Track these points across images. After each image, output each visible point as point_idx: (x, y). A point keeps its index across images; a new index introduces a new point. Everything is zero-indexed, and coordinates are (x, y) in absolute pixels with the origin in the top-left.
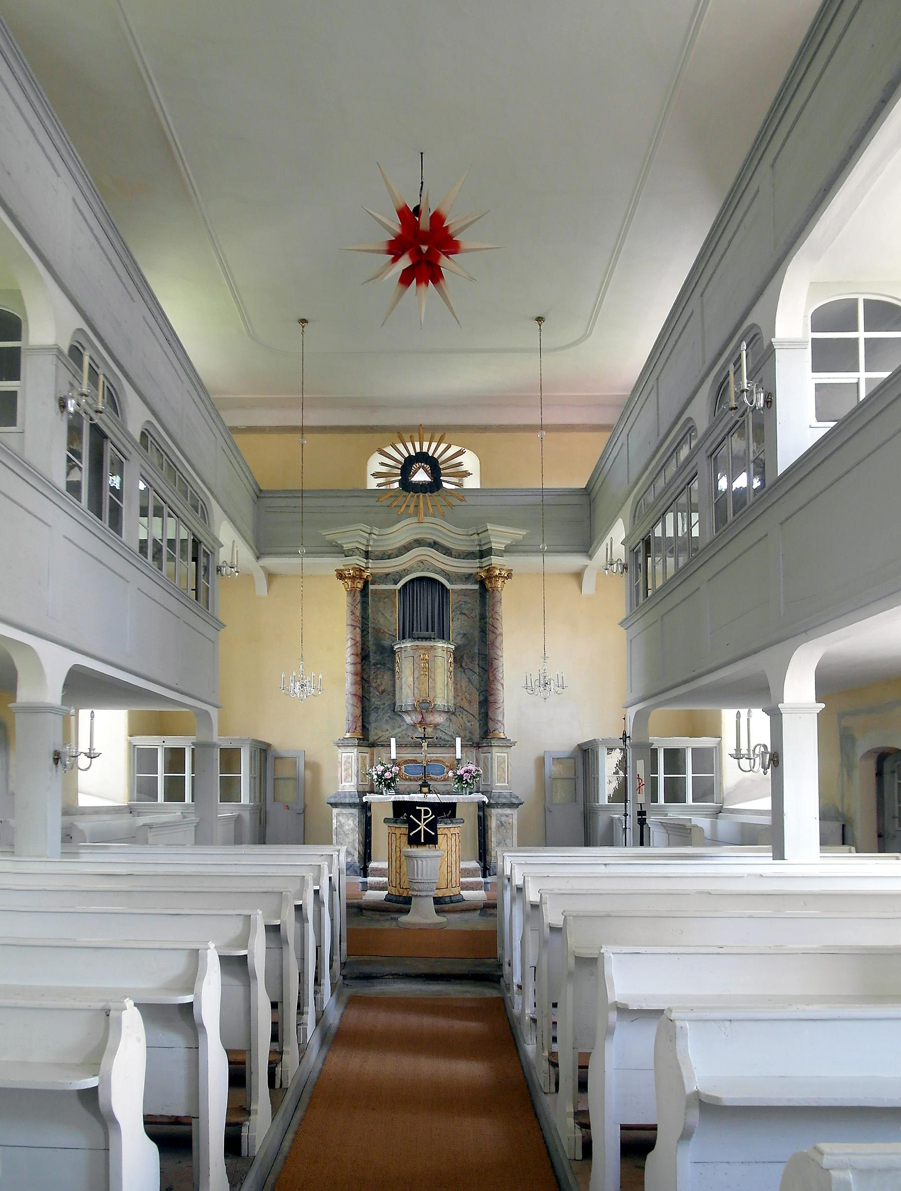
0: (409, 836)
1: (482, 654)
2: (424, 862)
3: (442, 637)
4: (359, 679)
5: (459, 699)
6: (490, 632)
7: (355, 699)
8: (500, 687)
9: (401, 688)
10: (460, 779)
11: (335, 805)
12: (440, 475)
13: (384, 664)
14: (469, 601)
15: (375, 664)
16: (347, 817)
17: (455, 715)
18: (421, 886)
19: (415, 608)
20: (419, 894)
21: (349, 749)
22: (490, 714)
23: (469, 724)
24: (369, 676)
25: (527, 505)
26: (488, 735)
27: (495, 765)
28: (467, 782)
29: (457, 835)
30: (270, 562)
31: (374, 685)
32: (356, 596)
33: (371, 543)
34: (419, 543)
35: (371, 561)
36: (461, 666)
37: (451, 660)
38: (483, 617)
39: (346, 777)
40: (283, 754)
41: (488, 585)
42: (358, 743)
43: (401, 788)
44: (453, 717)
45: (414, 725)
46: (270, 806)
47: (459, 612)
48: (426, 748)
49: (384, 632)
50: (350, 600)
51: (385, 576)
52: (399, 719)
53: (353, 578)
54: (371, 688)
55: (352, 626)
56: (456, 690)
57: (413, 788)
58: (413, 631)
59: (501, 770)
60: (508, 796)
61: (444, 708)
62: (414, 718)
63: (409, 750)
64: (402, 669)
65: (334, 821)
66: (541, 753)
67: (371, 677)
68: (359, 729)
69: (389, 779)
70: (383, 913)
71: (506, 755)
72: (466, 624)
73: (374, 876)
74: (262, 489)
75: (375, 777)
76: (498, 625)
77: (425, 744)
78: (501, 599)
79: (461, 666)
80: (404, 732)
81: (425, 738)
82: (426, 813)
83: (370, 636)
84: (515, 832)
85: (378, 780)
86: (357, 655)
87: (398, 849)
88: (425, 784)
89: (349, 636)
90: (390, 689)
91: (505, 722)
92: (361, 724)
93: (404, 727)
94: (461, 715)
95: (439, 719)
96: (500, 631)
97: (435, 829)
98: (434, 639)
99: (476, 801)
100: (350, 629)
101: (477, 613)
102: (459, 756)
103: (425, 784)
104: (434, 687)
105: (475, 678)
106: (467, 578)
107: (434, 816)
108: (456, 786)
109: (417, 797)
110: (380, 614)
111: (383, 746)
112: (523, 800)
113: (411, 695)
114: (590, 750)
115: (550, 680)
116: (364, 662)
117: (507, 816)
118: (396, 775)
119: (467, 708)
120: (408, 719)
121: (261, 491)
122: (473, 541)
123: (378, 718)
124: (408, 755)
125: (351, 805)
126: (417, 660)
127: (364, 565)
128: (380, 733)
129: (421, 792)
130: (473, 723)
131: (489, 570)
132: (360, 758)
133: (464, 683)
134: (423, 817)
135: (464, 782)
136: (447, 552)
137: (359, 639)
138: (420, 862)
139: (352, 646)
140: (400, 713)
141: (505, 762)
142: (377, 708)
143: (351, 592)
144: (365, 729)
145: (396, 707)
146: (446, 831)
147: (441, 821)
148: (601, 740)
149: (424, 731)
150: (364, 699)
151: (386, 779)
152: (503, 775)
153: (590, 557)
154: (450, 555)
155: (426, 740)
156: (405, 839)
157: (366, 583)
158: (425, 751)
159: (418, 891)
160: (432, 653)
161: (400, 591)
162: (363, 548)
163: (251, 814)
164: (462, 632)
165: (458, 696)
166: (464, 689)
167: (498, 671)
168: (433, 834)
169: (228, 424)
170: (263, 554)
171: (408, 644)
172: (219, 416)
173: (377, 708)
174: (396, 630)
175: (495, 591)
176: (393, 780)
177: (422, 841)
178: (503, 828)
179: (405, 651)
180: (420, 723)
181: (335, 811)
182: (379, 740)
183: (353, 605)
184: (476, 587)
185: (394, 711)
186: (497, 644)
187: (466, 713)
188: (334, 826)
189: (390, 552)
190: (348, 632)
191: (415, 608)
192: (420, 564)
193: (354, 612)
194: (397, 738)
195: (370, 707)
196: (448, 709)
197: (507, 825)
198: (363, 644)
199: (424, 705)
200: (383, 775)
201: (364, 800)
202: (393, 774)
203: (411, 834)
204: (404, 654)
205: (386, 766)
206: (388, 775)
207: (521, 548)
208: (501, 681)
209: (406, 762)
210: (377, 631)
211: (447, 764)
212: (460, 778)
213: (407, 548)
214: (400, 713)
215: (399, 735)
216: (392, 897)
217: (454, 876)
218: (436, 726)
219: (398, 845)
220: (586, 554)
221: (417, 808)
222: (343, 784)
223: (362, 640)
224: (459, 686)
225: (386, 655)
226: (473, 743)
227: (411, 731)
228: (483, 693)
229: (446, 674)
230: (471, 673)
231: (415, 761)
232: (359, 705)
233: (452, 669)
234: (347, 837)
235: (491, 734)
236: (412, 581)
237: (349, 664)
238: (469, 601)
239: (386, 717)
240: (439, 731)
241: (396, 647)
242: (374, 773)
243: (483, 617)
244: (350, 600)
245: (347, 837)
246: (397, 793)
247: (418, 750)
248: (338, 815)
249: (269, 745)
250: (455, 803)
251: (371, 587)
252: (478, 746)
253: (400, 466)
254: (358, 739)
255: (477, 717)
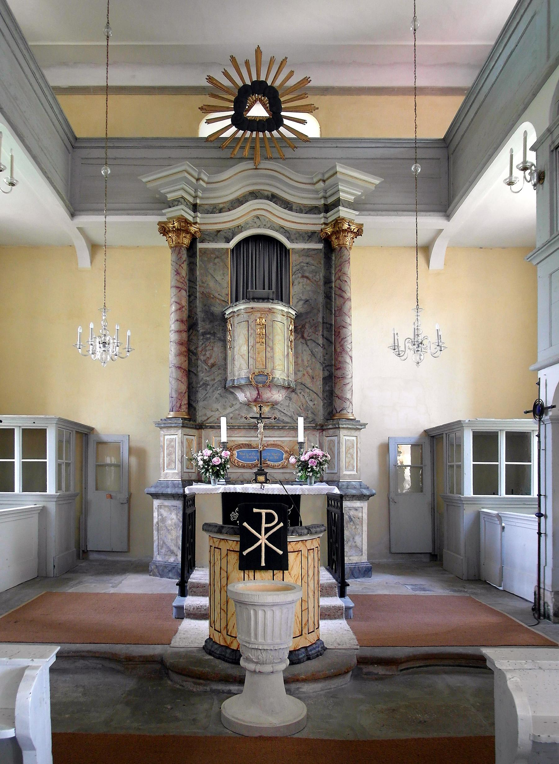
0: (241, 557)
1: (326, 323)
2: (269, 614)
3: (280, 298)
4: (184, 349)
5: (300, 374)
6: (337, 296)
7: (179, 373)
8: (348, 360)
9: (233, 359)
10: (304, 466)
11: (156, 496)
12: (280, 110)
13: (214, 334)
14: (312, 262)
15: (204, 334)
16: (170, 510)
17: (296, 393)
18: (263, 656)
19: (250, 277)
20: (258, 668)
21: (172, 431)
22: (337, 392)
23: (311, 404)
24: (197, 347)
25: (377, 159)
26: (334, 415)
27: (343, 449)
28: (312, 470)
29: (316, 550)
30: (84, 220)
31: (202, 358)
32: (182, 253)
33: (200, 194)
34: (254, 195)
35: (199, 215)
36: (303, 337)
37: (292, 327)
38: (328, 281)
39: (169, 464)
40: (105, 439)
41: (335, 242)
42: (183, 423)
43: (233, 477)
44: (293, 395)
45: (248, 404)
46: (92, 494)
47: (300, 275)
48: (263, 431)
49: (215, 297)
50: (174, 257)
51: (216, 233)
52: (231, 397)
53: (178, 231)
54: (199, 362)
55: (177, 287)
56: (296, 363)
57: (247, 476)
58: (247, 288)
59: (349, 456)
60: (358, 486)
61: (284, 383)
62: (248, 394)
63: (243, 432)
64: (234, 337)
65: (155, 514)
66: (385, 439)
67: (200, 349)
68: (184, 408)
69: (218, 466)
70: (198, 681)
71: (354, 438)
72: (308, 288)
73: (195, 594)
74: (78, 136)
75: (201, 463)
76: (346, 288)
77: (261, 425)
78: (349, 259)
79: (303, 337)
80: (237, 412)
81: (260, 418)
82: (270, 518)
83: (198, 302)
84: (365, 528)
85: (204, 466)
86: (182, 321)
87: (224, 574)
88: (261, 472)
89: (173, 300)
90: (220, 362)
91: (354, 401)
92: (186, 402)
93: (237, 406)
94: (302, 393)
95: (278, 396)
96: (348, 294)
97: (283, 545)
98: (273, 300)
99: (325, 492)
100: (174, 291)
101: (320, 276)
102: (301, 438)
103: (261, 472)
104: (272, 357)
105: (319, 351)
106: (310, 237)
107: (281, 524)
108: (300, 474)
109: (252, 488)
110: (210, 277)
111: (212, 427)
112: (374, 491)
113: (244, 366)
114: (444, 435)
115: (426, 338)
116: (191, 331)
117: (356, 510)
118: (226, 461)
119: (309, 384)
120: (241, 397)
121: (76, 139)
122: (317, 192)
123: (207, 395)
124: (241, 438)
125: (174, 496)
126: (252, 325)
127: (190, 219)
128: (209, 414)
129: (256, 481)
130: (316, 403)
131: (338, 222)
132: (185, 441)
133: (306, 356)
134: (264, 525)
135: (309, 470)
136: (287, 205)
137: (184, 303)
138: (260, 614)
139: (176, 310)
140: (231, 390)
141: (353, 447)
142: (206, 384)
143: (176, 248)
144: (191, 407)
145: (228, 382)
146: (300, 546)
147: (293, 532)
148: (467, 421)
149: (260, 410)
150: (191, 373)
151: (215, 466)
152: (351, 462)
153: (448, 217)
154: (291, 209)
155: (263, 420)
156: (234, 559)
157: (194, 240)
158: (262, 434)
159: (257, 663)
160: (270, 317)
161: (232, 251)
162: (191, 200)
163: (58, 505)
164: (303, 298)
165: (299, 371)
166: (306, 363)
167: (346, 341)
168: (281, 552)
169: (52, 84)
170: (80, 211)
171: (242, 306)
172: (43, 76)
173: (206, 384)
174: (227, 295)
175: (343, 249)
176: (222, 466)
177: (263, 564)
178: (352, 523)
179: (238, 315)
180: (255, 401)
181: (156, 503)
182: (208, 421)
183: (177, 263)
184: (320, 246)
185: (225, 388)
186: (346, 309)
187: (308, 391)
188: (155, 521)
189: (221, 206)
190: (173, 295)
191: (250, 277)
192: (256, 220)
193: (179, 271)
194: (229, 419)
195: (197, 383)
196: (289, 385)
197: (357, 521)
198: (190, 311)
199: (259, 377)
200: (210, 460)
201: (187, 491)
202: (223, 460)
203: (245, 553)
204: (236, 320)
205: (214, 450)
206: (216, 461)
207: (368, 206)
208: (350, 353)
209: (239, 446)
210: (207, 296)
211: (286, 449)
212: (304, 466)
213: (239, 202)
214: (231, 390)
215: (231, 415)
216: (216, 646)
217: (311, 614)
218: (274, 405)
219: (224, 567)
220: (443, 213)
221: (255, 510)
222: (166, 471)
223: (190, 306)
224: (300, 359)
225: (216, 323)
226: (316, 425)
227: (245, 411)
228: (328, 368)
229: (286, 343)
230: (314, 344)
231: (249, 446)
232: (185, 379)
233: (292, 338)
234: (169, 533)
235: (338, 415)
236: (246, 240)
237: (173, 332)
238: (312, 262)
239: (216, 394)
240: (276, 411)
241: (227, 312)
242: (199, 458)
243: (328, 281)
244: (174, 258)
245: (169, 533)
246: (228, 482)
247: (252, 433)
248: (160, 507)
249: (91, 429)
250: (299, 496)
251: (200, 246)
252: (322, 428)
253: (233, 98)
254: (182, 419)
255: (321, 395)
